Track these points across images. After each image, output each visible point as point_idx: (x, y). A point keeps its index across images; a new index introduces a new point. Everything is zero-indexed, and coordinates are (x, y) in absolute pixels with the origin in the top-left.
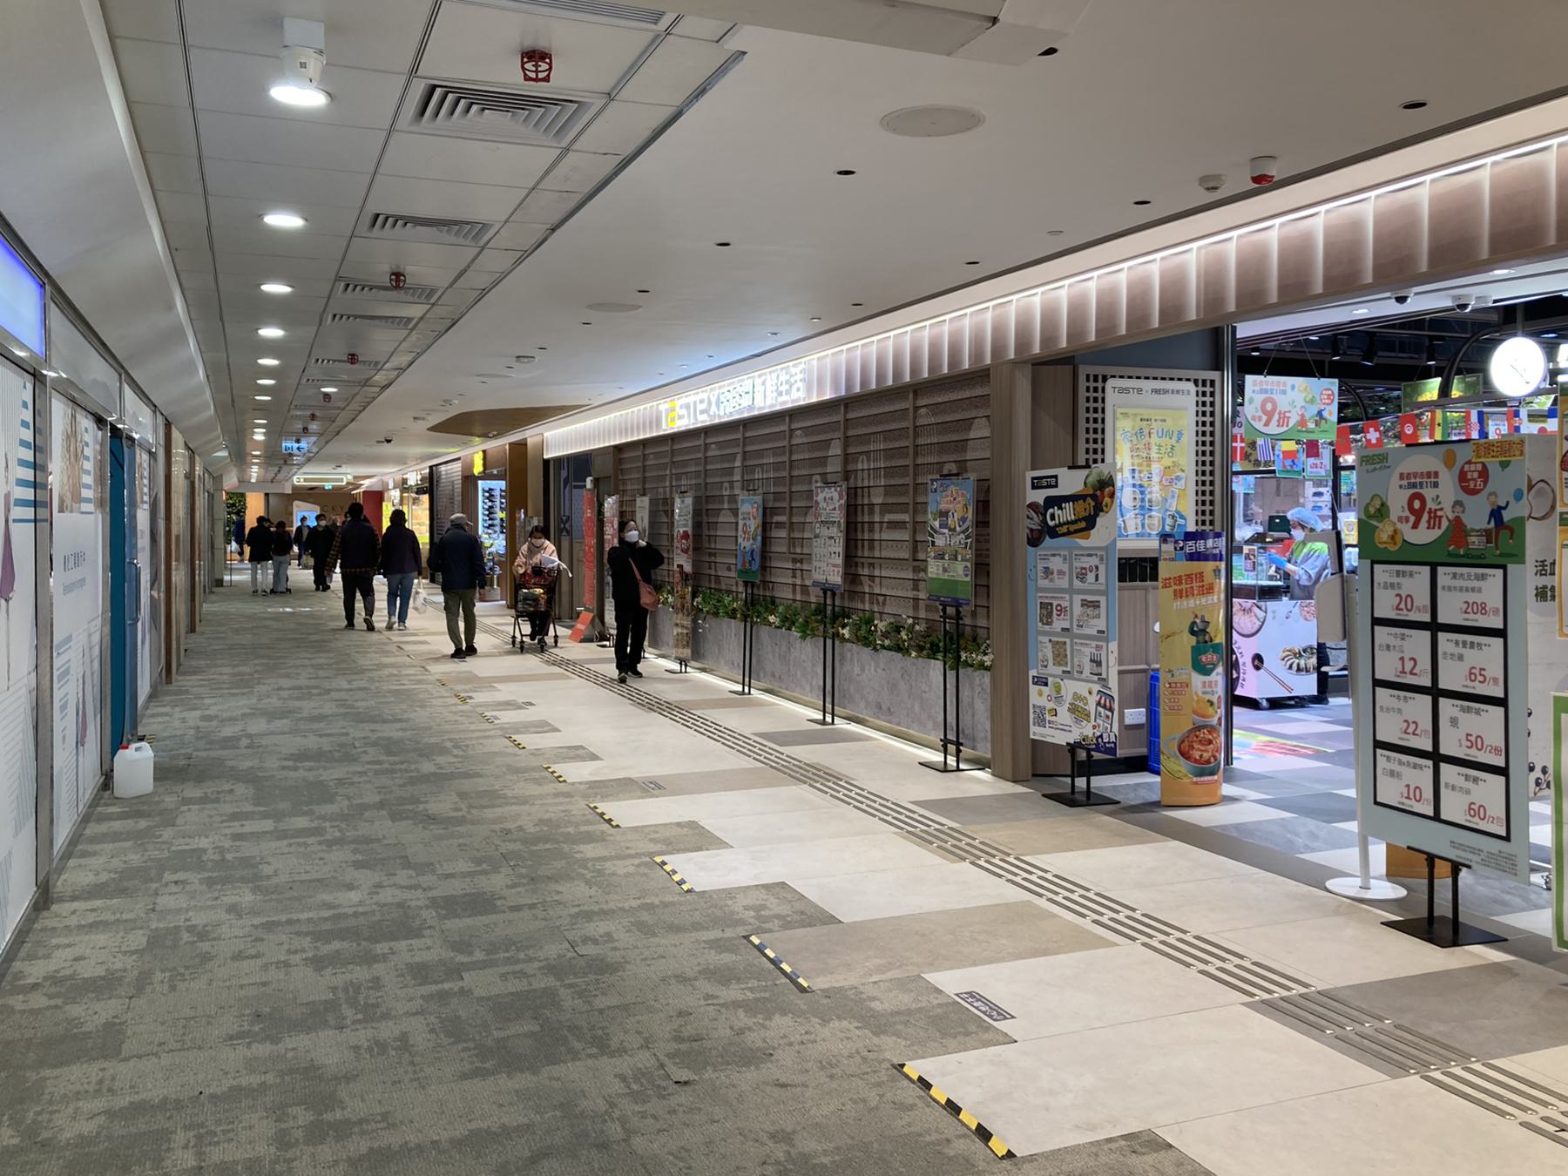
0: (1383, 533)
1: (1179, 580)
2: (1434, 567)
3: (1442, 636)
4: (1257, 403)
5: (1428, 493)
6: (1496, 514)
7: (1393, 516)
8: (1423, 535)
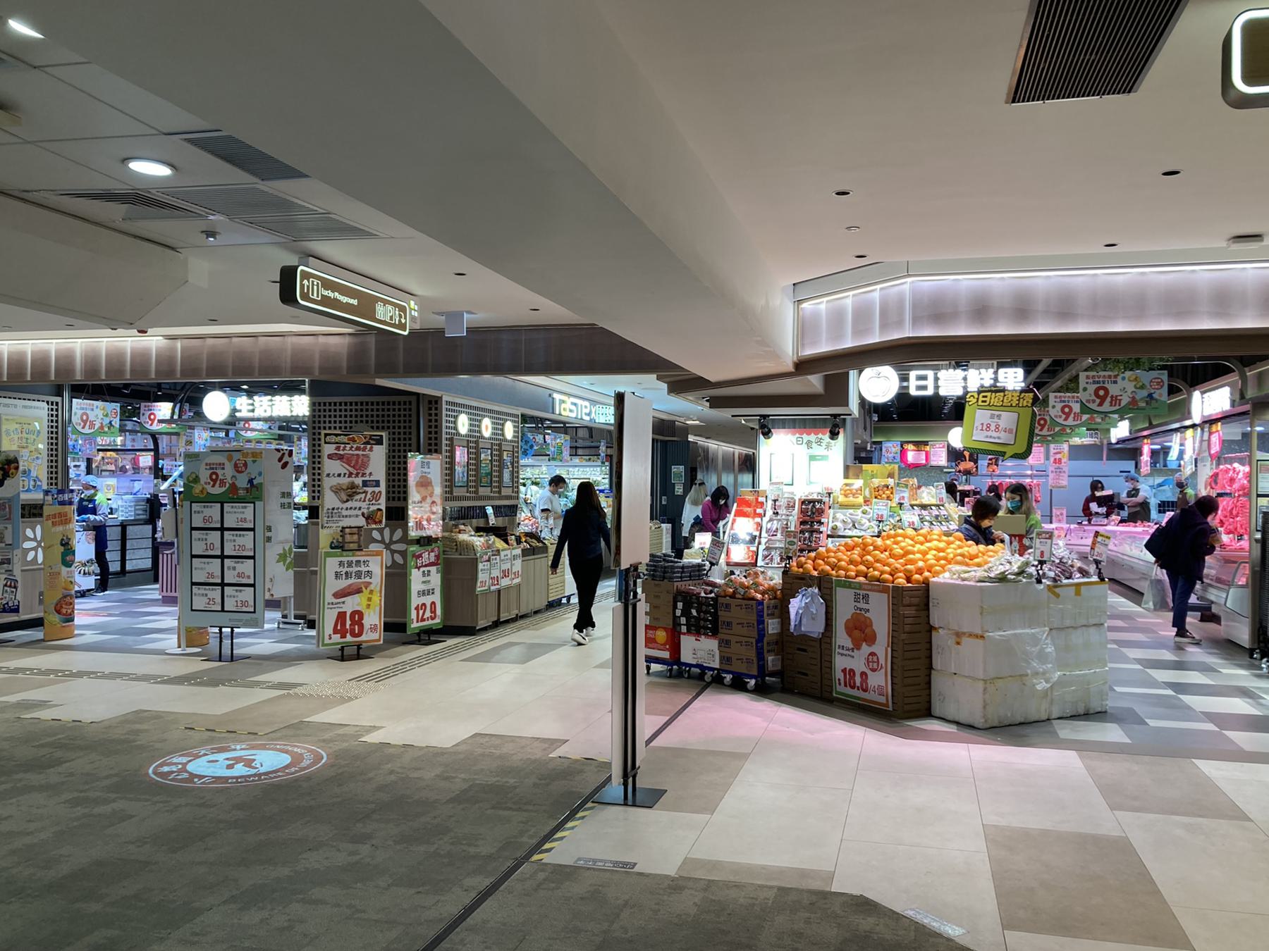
0: (197, 489)
1: (54, 516)
2: (123, 571)
3: (226, 533)
4: (79, 416)
5: (220, 472)
6: (251, 481)
7: (202, 482)
8: (217, 490)
